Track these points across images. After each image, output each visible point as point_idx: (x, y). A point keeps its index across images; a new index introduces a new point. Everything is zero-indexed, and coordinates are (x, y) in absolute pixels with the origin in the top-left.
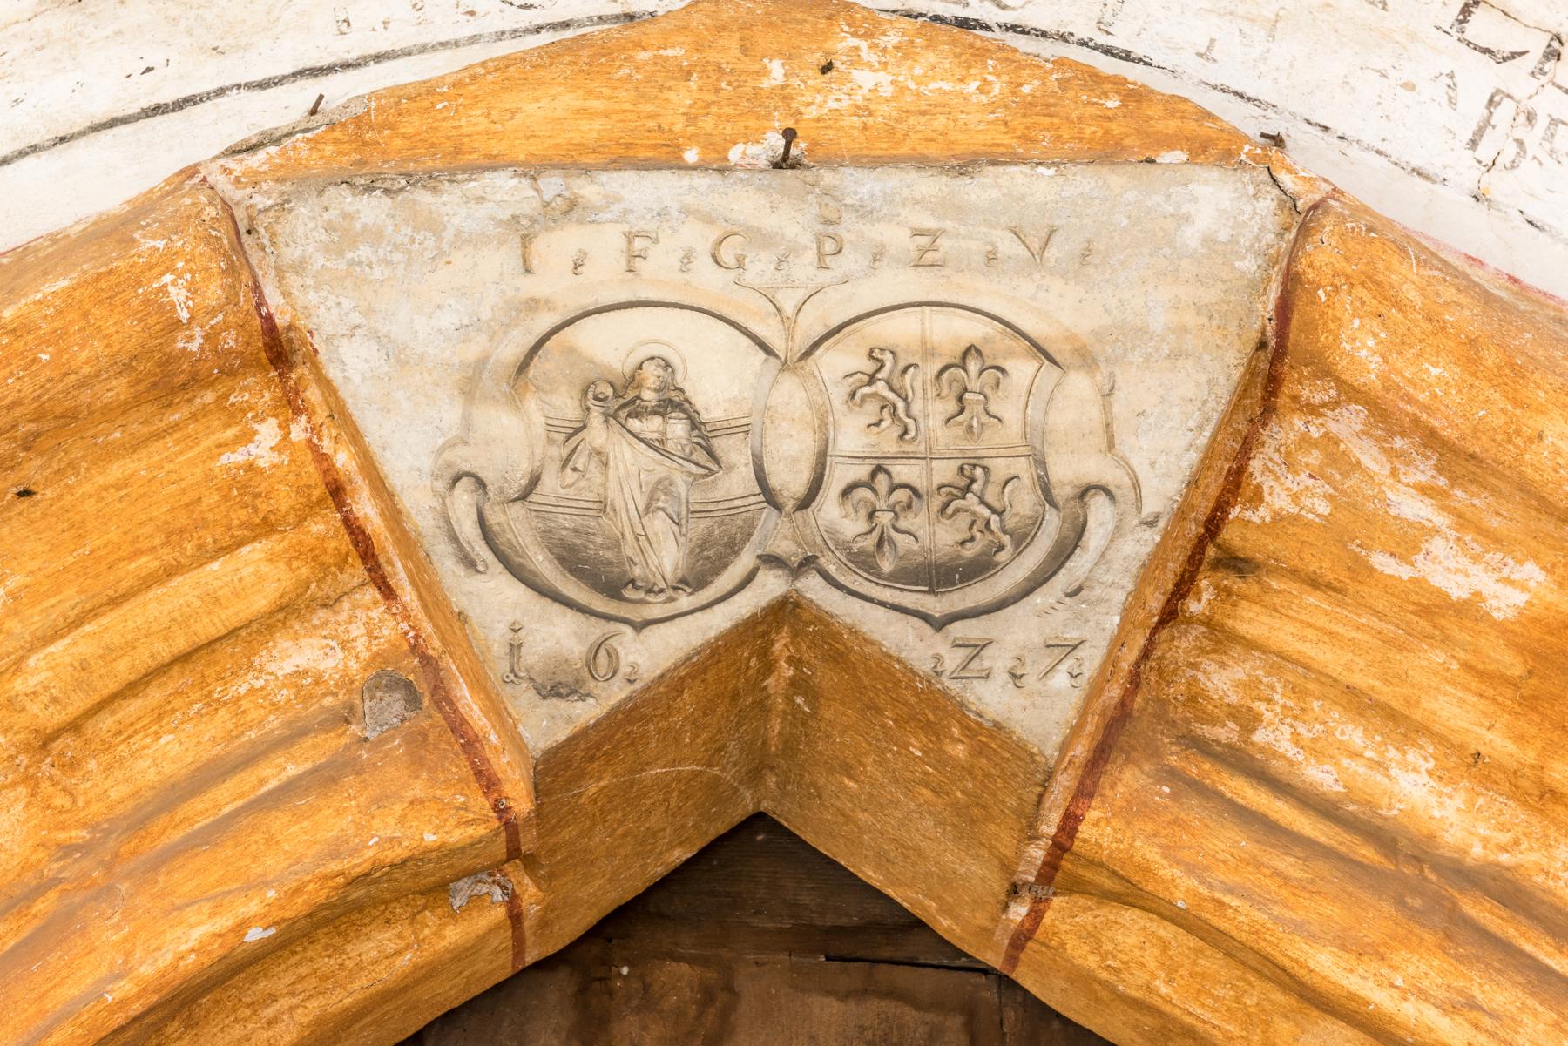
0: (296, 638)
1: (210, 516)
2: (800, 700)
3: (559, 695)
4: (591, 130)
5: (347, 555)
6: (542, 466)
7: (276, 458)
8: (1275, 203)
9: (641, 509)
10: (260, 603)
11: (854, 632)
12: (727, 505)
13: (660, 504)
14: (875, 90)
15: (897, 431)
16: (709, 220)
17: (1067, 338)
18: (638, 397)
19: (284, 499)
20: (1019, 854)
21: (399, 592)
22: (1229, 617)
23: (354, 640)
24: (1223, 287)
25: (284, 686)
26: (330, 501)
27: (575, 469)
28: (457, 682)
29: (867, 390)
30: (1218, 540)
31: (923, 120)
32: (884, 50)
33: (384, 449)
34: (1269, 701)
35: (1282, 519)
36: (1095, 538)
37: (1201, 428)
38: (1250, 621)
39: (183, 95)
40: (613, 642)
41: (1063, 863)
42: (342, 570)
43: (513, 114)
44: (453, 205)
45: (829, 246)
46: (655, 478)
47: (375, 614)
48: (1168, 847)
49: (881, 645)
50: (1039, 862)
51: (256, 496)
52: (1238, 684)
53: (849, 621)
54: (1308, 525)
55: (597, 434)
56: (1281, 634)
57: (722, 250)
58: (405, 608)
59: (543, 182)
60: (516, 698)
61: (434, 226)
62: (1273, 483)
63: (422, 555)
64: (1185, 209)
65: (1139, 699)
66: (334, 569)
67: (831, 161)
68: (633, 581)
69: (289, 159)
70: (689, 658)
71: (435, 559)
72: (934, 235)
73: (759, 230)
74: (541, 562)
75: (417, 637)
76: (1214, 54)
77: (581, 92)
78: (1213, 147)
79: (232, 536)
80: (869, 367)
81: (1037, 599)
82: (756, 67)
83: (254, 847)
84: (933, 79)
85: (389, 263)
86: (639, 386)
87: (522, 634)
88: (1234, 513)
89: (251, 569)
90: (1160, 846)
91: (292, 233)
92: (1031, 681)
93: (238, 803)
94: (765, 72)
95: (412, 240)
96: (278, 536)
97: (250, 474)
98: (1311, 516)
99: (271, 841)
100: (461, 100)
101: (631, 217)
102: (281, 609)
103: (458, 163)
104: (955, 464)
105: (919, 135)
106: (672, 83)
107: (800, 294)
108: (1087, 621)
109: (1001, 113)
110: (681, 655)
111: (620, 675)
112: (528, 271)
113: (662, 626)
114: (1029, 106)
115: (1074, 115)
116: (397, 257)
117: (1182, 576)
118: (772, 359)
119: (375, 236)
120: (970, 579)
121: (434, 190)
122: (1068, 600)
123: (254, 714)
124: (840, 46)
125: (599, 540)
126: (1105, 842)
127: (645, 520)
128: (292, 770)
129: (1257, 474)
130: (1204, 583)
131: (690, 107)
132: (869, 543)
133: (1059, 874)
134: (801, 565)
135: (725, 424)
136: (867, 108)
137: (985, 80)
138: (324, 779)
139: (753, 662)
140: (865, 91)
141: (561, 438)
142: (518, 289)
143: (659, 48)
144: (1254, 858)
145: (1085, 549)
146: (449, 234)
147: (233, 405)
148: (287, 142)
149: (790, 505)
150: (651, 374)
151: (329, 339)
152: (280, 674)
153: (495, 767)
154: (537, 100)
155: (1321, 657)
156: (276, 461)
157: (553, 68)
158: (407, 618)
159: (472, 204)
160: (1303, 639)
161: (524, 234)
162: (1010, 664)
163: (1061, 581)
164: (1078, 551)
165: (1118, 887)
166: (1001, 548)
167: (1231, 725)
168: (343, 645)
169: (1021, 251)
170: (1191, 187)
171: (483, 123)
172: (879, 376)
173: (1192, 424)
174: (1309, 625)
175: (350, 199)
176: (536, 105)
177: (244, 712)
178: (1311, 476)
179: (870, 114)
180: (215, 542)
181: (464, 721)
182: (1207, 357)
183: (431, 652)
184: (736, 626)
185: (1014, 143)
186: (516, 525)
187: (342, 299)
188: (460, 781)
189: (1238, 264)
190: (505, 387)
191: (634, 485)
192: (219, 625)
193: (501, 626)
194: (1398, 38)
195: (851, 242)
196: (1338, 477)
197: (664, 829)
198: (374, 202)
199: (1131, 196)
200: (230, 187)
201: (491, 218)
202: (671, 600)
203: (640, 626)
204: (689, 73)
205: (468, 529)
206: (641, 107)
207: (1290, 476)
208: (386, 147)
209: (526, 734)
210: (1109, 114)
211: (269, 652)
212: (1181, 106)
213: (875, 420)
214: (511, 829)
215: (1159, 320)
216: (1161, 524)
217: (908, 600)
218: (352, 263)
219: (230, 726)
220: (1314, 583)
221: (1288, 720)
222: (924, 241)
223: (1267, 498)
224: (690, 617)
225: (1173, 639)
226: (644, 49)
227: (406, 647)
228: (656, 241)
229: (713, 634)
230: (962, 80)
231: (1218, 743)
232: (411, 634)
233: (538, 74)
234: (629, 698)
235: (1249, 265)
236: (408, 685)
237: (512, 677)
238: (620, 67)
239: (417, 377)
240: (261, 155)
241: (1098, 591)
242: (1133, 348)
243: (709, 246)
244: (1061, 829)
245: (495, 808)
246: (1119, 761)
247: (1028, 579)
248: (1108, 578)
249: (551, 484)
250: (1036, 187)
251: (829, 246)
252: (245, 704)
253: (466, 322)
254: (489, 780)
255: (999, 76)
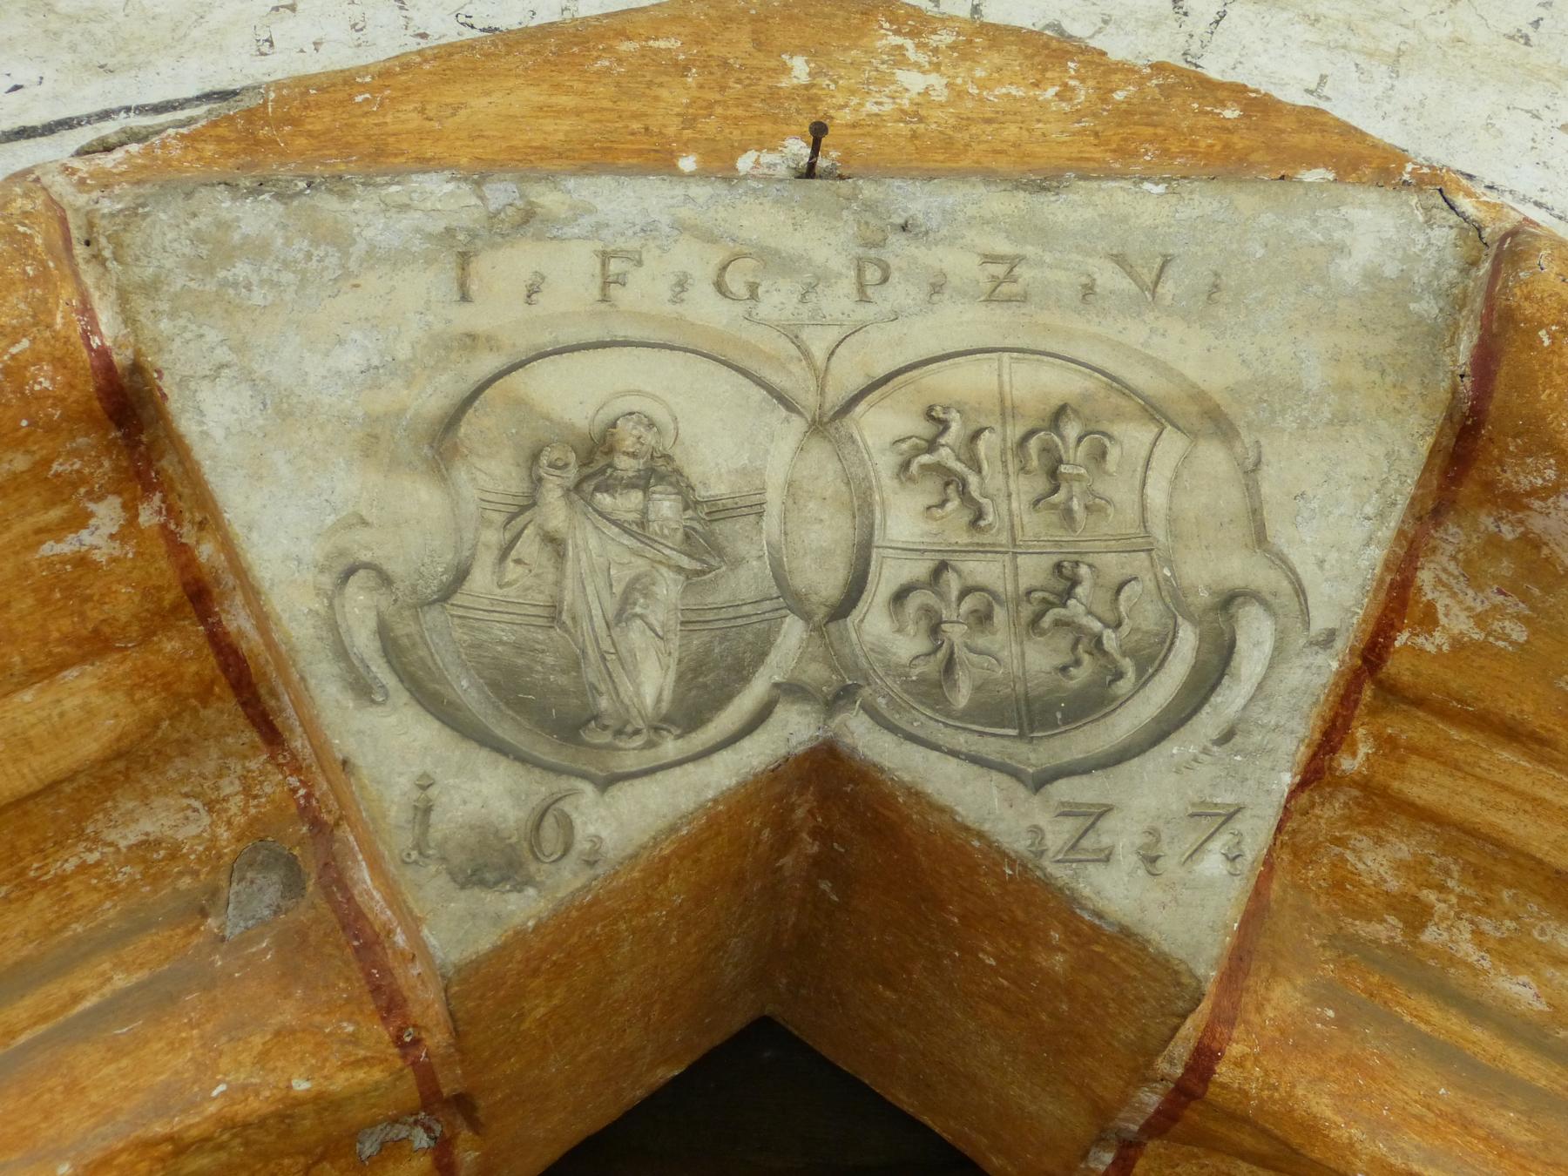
0: (145, 797)
1: (19, 627)
2: (825, 886)
3: (483, 883)
4: (557, 130)
5: (213, 682)
6: (473, 556)
7: (116, 549)
8: (1453, 233)
9: (610, 616)
10: (89, 747)
11: (915, 794)
12: (732, 613)
13: (638, 610)
14: (926, 92)
15: (966, 516)
16: (709, 237)
17: (1191, 397)
18: (610, 465)
19: (123, 603)
20: (1125, 1100)
21: (286, 735)
22: (1394, 776)
23: (226, 799)
24: (1397, 335)
25: (127, 862)
26: (189, 608)
27: (518, 561)
28: (356, 861)
29: (925, 459)
30: (1381, 675)
31: (989, 128)
32: (936, 50)
33: (250, 529)
34: (1442, 888)
35: (1463, 646)
36: (1251, 661)
37: (1381, 515)
38: (1424, 782)
39: (56, 118)
40: (566, 806)
41: (1187, 1112)
42: (205, 704)
43: (456, 110)
44: (369, 216)
45: (871, 273)
46: (628, 574)
47: (253, 765)
48: (1342, 1096)
49: (952, 812)
50: (1151, 1110)
51: (87, 599)
52: (1400, 866)
53: (907, 778)
54: (1498, 655)
55: (555, 512)
56: (1466, 801)
57: (727, 277)
58: (294, 757)
59: (487, 190)
60: (420, 887)
61: (340, 240)
62: (1448, 601)
63: (296, 677)
64: (1337, 235)
65: (1275, 886)
66: (193, 702)
67: (879, 171)
68: (595, 718)
69: (157, 158)
70: (673, 829)
71: (312, 682)
72: (1014, 261)
73: (777, 252)
74: (465, 689)
75: (308, 796)
76: (1326, 91)
77: (545, 86)
78: (1369, 164)
79: (50, 654)
80: (925, 429)
81: (1172, 748)
82: (773, 64)
83: (47, 1097)
84: (1000, 82)
85: (275, 285)
86: (611, 451)
87: (433, 792)
88: (1402, 639)
89: (77, 701)
90: (1331, 1094)
91: (144, 245)
92: (1170, 863)
93: (42, 1029)
94: (786, 70)
95: (309, 256)
96: (117, 656)
97: (80, 571)
98: (1501, 644)
99: (73, 1089)
100: (387, 92)
101: (605, 233)
102: (119, 755)
103: (380, 159)
104: (1048, 562)
105: (984, 146)
106: (664, 79)
107: (833, 334)
108: (1244, 780)
109: (1088, 123)
110: (661, 824)
111: (574, 854)
112: (465, 297)
113: (637, 782)
114: (1125, 114)
115: (1184, 125)
116: (287, 277)
117: (1333, 721)
118: (794, 417)
119: (258, 250)
120: (1076, 720)
121: (343, 195)
122: (1215, 749)
123: (85, 900)
124: (878, 44)
125: (550, 660)
126: (1253, 1088)
127: (616, 632)
128: (121, 981)
129: (1427, 588)
130: (1360, 732)
131: (688, 106)
132: (931, 668)
133: (1178, 1126)
134: (837, 697)
135: (730, 504)
136: (916, 114)
137: (1066, 85)
138: (156, 1000)
139: (766, 833)
140: (913, 94)
141: (499, 518)
142: (449, 321)
143: (648, 39)
144: (1460, 1112)
145: (1236, 678)
146: (359, 249)
147: (57, 475)
148: (156, 140)
149: (820, 614)
150: (628, 435)
151: (183, 382)
152: (123, 844)
153: (401, 981)
154: (487, 94)
155: (1521, 832)
156: (116, 553)
157: (510, 58)
158: (297, 770)
159: (393, 213)
160: (1496, 807)
161: (461, 253)
162: (1139, 840)
163: (1207, 723)
164: (1226, 681)
165: (1265, 1148)
166: (1119, 675)
167: (1392, 920)
168: (210, 806)
169: (1125, 284)
170: (1343, 210)
171: (415, 121)
172: (942, 441)
173: (1369, 510)
174: (1504, 788)
175: (227, 204)
176: (485, 101)
177: (70, 897)
178: (1500, 592)
179: (921, 120)
180: (25, 661)
181: (360, 915)
182: (1381, 423)
183: (325, 817)
184: (743, 784)
185: (1108, 157)
186: (441, 641)
187: (205, 330)
188: (348, 1001)
189: (1412, 306)
190: (426, 450)
191: (601, 582)
192: (31, 777)
193: (403, 780)
194: (1549, 75)
195: (900, 269)
196: (1536, 592)
197: (644, 1048)
198: (260, 208)
199: (1267, 219)
200: (70, 189)
201: (417, 230)
202: (650, 744)
203: (608, 782)
204: (687, 68)
205: (364, 641)
206: (622, 105)
207: (1471, 593)
208: (274, 139)
209: (432, 941)
210: (1229, 125)
211: (106, 812)
212: (1318, 118)
213: (935, 500)
214: (426, 1076)
215: (1315, 376)
216: (1340, 644)
217: (989, 748)
218: (224, 283)
219: (49, 916)
220: (1511, 733)
221: (1467, 915)
222: (1000, 270)
223: (1443, 620)
224: (678, 771)
225: (1313, 806)
226: (629, 39)
227: (293, 810)
228: (640, 263)
229: (710, 794)
230: (1036, 85)
231: (1376, 942)
232: (302, 792)
233: (489, 65)
234: (586, 888)
235: (1427, 307)
236: (291, 863)
237: (415, 855)
238: (598, 58)
239: (304, 433)
240: (119, 154)
241: (1257, 738)
242: (1283, 411)
243: (711, 271)
244: (1189, 1069)
245: (398, 1040)
246: (1264, 974)
247: (1156, 720)
248: (1271, 719)
249: (481, 579)
250: (1146, 206)
251: (871, 273)
252: (73, 886)
253: (375, 361)
254: (391, 1000)
255: (1083, 81)
